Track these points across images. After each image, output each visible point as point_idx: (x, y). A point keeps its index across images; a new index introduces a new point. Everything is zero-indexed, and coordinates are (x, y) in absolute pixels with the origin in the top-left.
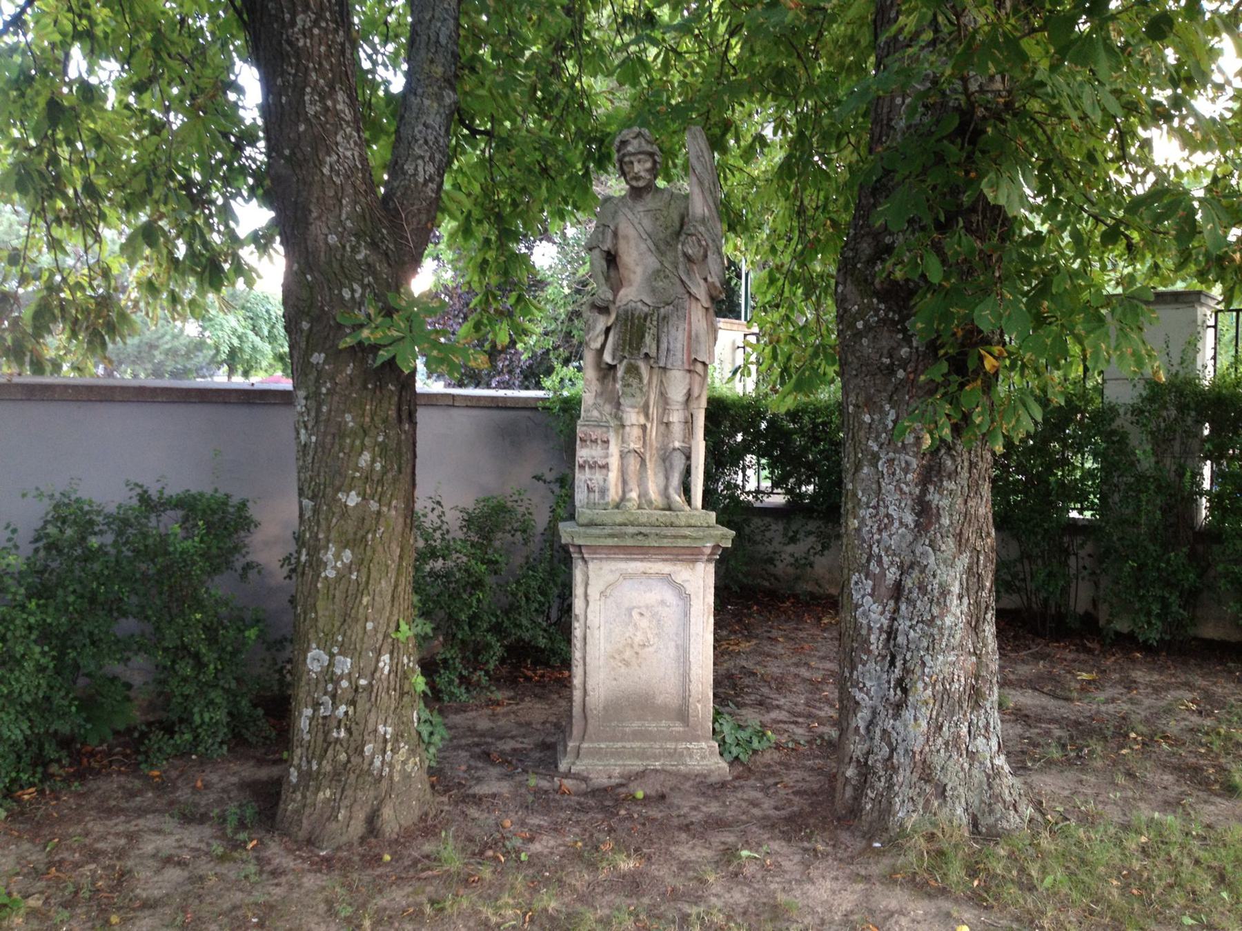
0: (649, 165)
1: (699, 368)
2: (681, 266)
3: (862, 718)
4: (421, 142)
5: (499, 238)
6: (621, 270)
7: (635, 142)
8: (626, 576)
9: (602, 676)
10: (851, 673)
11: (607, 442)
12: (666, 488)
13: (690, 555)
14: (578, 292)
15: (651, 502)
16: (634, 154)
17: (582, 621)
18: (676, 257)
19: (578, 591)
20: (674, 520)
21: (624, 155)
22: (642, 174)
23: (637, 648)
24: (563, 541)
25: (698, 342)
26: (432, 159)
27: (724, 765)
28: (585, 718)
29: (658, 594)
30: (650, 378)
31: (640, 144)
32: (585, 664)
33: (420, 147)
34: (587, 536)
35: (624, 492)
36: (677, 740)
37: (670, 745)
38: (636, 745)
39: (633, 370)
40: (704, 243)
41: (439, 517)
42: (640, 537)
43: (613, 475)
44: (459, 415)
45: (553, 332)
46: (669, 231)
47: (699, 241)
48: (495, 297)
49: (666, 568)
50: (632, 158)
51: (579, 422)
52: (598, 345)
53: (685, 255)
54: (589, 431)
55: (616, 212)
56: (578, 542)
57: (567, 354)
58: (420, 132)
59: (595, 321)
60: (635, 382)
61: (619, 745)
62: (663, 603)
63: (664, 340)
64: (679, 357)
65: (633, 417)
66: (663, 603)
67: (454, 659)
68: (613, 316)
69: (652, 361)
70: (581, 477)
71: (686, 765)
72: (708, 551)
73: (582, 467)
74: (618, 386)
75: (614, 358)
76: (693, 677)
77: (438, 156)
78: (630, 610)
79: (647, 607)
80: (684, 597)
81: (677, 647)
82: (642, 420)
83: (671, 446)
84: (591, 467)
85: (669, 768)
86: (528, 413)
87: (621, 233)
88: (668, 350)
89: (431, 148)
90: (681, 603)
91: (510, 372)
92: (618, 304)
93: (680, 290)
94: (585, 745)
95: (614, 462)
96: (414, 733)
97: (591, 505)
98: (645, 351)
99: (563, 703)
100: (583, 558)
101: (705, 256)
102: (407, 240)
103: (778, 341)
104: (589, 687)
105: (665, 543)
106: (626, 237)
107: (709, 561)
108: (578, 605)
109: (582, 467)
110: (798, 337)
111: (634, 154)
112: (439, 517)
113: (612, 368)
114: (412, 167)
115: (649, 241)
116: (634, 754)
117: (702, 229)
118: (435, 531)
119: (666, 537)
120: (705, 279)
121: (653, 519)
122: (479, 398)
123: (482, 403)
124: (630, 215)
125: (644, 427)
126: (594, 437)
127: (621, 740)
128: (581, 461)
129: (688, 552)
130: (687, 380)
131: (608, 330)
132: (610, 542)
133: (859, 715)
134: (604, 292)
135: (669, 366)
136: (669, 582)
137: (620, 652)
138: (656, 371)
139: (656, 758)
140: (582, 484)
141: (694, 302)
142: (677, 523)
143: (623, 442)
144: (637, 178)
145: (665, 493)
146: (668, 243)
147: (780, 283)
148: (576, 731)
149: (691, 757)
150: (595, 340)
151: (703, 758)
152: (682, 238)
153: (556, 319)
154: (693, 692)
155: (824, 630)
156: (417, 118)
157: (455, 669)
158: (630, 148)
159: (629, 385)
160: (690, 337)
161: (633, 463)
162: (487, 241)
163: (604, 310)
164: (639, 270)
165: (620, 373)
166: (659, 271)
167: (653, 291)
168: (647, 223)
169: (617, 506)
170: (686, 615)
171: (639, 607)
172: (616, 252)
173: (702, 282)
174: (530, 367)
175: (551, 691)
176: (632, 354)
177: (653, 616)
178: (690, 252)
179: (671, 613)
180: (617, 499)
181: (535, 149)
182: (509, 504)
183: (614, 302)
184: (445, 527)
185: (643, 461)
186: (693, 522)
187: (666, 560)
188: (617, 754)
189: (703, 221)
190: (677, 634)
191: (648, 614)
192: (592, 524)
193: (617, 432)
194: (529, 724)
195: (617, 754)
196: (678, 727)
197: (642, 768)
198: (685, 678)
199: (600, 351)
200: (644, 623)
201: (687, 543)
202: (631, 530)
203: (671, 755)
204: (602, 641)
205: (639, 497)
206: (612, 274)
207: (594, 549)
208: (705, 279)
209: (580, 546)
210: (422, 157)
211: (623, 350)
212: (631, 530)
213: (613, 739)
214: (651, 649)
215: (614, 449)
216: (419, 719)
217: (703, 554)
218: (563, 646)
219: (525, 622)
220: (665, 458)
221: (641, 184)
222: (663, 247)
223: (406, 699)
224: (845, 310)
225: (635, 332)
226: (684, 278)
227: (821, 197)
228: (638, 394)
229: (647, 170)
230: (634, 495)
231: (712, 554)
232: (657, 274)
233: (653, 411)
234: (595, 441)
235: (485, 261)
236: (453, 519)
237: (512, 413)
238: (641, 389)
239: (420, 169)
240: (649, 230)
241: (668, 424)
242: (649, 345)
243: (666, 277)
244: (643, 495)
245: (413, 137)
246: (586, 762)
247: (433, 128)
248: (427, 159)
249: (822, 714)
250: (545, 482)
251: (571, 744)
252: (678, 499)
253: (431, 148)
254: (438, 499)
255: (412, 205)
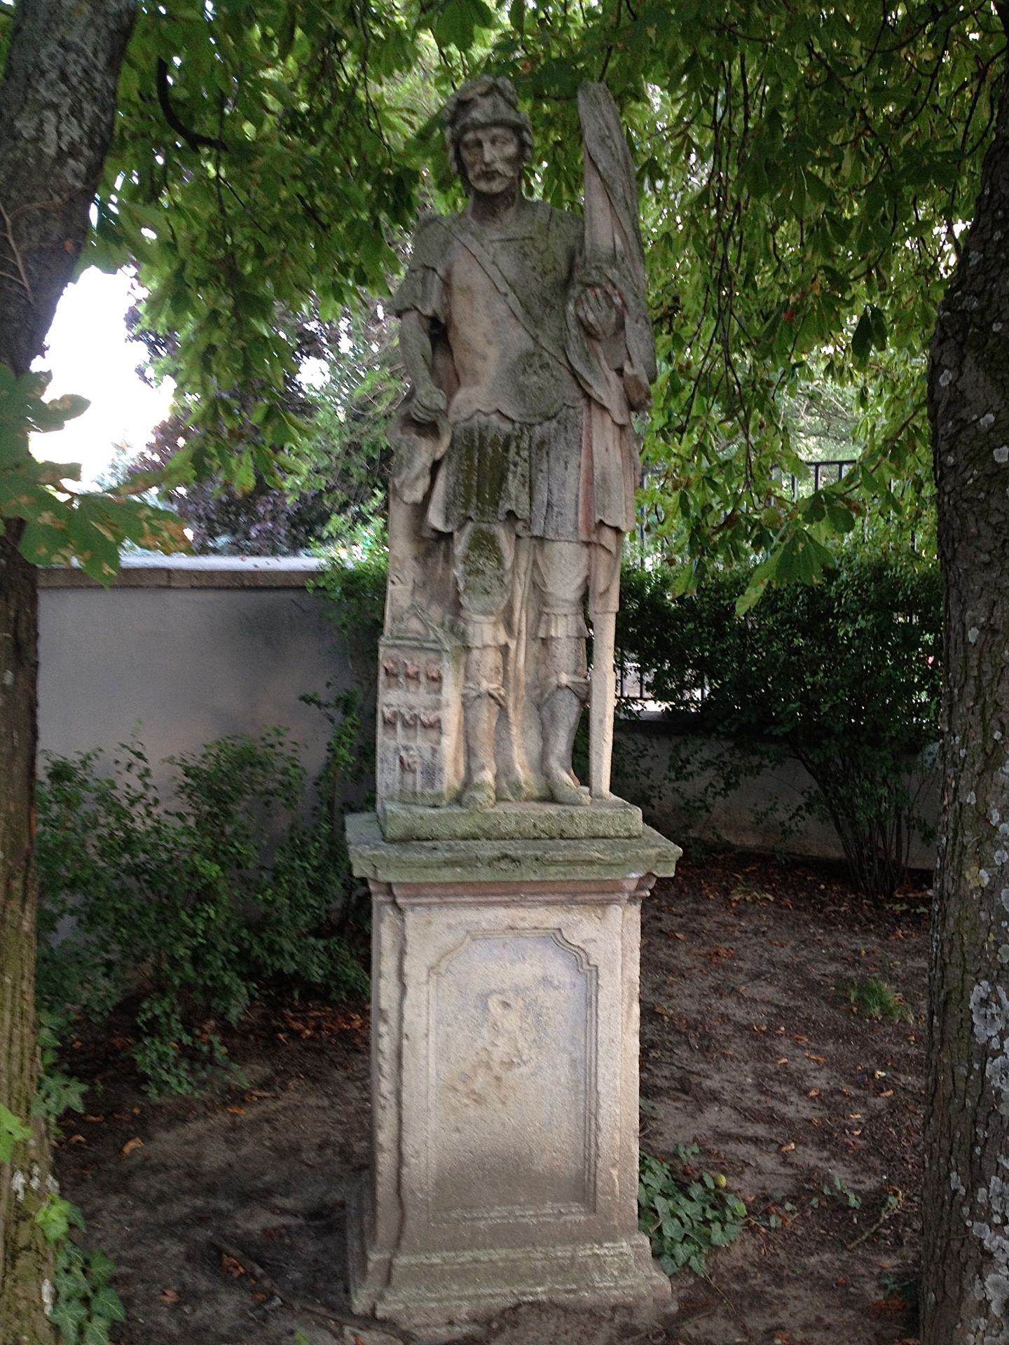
0: (511, 150)
1: (608, 538)
2: (573, 347)
3: (996, 1285)
4: (53, 75)
5: (235, 311)
6: (457, 353)
7: (486, 103)
8: (475, 935)
9: (433, 1125)
10: (972, 1191)
11: (438, 680)
12: (544, 757)
13: (599, 895)
14: (356, 418)
15: (519, 788)
16: (484, 126)
17: (393, 1021)
18: (564, 329)
19: (386, 964)
20: (565, 825)
21: (465, 129)
22: (500, 166)
23: (498, 1070)
24: (356, 873)
25: (607, 491)
26: (76, 111)
27: (662, 1280)
28: (401, 1204)
29: (536, 966)
30: (516, 557)
31: (495, 106)
32: (399, 1103)
33: (52, 85)
34: (402, 865)
35: (469, 769)
36: (575, 1239)
37: (562, 1252)
38: (499, 1254)
39: (484, 543)
40: (617, 300)
41: (141, 777)
42: (503, 865)
43: (450, 743)
44: (180, 603)
45: (326, 469)
46: (549, 279)
47: (608, 296)
48: (229, 410)
49: (551, 917)
50: (480, 135)
51: (383, 640)
52: (417, 495)
53: (581, 323)
54: (402, 657)
55: (447, 243)
56: (383, 876)
57: (345, 498)
58: (52, 57)
59: (412, 449)
60: (489, 566)
61: (467, 1256)
62: (546, 981)
63: (542, 485)
64: (570, 515)
65: (485, 631)
66: (546, 981)
67: (167, 1015)
68: (446, 441)
69: (519, 526)
70: (386, 743)
71: (593, 1289)
72: (632, 886)
73: (389, 724)
74: (457, 572)
75: (447, 520)
76: (604, 1120)
77: (89, 108)
78: (484, 998)
79: (517, 991)
80: (584, 966)
81: (573, 1063)
82: (503, 637)
83: (553, 680)
84: (406, 725)
85: (563, 1298)
86: (292, 595)
87: (456, 282)
88: (549, 505)
89: (73, 89)
90: (580, 981)
91: (274, 519)
92: (452, 418)
93: (572, 392)
94: (402, 1260)
95: (451, 717)
96: (43, 1329)
97: (409, 798)
98: (508, 507)
99: (353, 1092)
100: (394, 903)
101: (621, 326)
102: (16, 272)
103: (687, 486)
104: (407, 1150)
105: (553, 873)
106: (468, 290)
107: (632, 900)
108: (385, 992)
109: (389, 724)
110: (719, 480)
111: (484, 126)
112: (141, 777)
113: (445, 538)
114: (32, 124)
115: (512, 297)
116: (497, 1274)
117: (613, 273)
118: (132, 803)
119: (554, 863)
120: (620, 371)
121: (527, 825)
122: (211, 574)
123: (217, 582)
124: (475, 247)
125: (504, 650)
126: (411, 670)
127: (473, 1245)
128: (388, 713)
129: (593, 887)
130: (584, 560)
131: (435, 467)
132: (447, 875)
133: (990, 1278)
134: (428, 393)
135: (551, 535)
136: (558, 943)
137: (466, 1078)
138: (526, 543)
139: (538, 1277)
140: (390, 756)
141: (595, 411)
142: (571, 830)
143: (467, 678)
144: (489, 175)
145: (542, 765)
146: (546, 302)
147: (686, 394)
148: (384, 1229)
149: (602, 1271)
150: (412, 486)
151: (624, 1271)
152: (575, 292)
153: (328, 453)
154: (604, 1148)
155: (739, 915)
156: (47, 30)
157: (171, 1032)
158: (477, 115)
159: (479, 572)
160: (590, 481)
161: (486, 717)
162: (214, 315)
163: (429, 429)
164: (493, 353)
165: (460, 547)
166: (530, 355)
167: (521, 392)
168: (507, 263)
169: (458, 800)
170: (588, 1003)
171: (502, 992)
172: (449, 318)
173: (613, 376)
174: (298, 512)
175: (333, 1063)
176: (482, 512)
177: (527, 1007)
178: (591, 317)
179: (560, 1002)
180: (457, 785)
181: (295, 177)
182: (260, 752)
183: (445, 413)
184: (151, 794)
185: (503, 709)
186: (600, 828)
187: (548, 903)
188: (463, 1274)
189: (613, 259)
190: (573, 1040)
191: (518, 1004)
192: (409, 839)
193: (456, 660)
194: (296, 1150)
195: (463, 1274)
196: (577, 1215)
197: (511, 1301)
198: (589, 1120)
199: (421, 508)
200: (511, 1021)
201: (592, 873)
202: (488, 849)
203: (562, 1270)
204: (432, 1060)
205: (496, 777)
206: (441, 362)
207: (416, 889)
208: (620, 371)
209: (389, 885)
210: (55, 107)
211: (466, 506)
212: (488, 849)
213: (454, 1245)
214: (524, 1070)
215: (451, 693)
216: (56, 1296)
217: (621, 890)
218: (352, 972)
219: (288, 946)
220: (542, 704)
221: (497, 186)
222: (537, 311)
223: (24, 1261)
224: (963, 424)
225: (487, 472)
226: (578, 366)
227: (743, 262)
228: (496, 590)
229: (508, 160)
230: (488, 776)
231: (640, 888)
232: (527, 361)
233: (521, 618)
234: (415, 677)
235: (211, 349)
236: (165, 775)
237: (265, 596)
238: (500, 580)
239: (49, 129)
240: (511, 274)
241: (546, 642)
242: (515, 494)
243: (545, 366)
244: (504, 771)
245: (36, 66)
246: (404, 1293)
247: (80, 52)
248: (65, 110)
249: (789, 1111)
250: (319, 704)
251: (375, 1257)
252: (566, 778)
253: (73, 89)
254: (138, 748)
255: (30, 200)
